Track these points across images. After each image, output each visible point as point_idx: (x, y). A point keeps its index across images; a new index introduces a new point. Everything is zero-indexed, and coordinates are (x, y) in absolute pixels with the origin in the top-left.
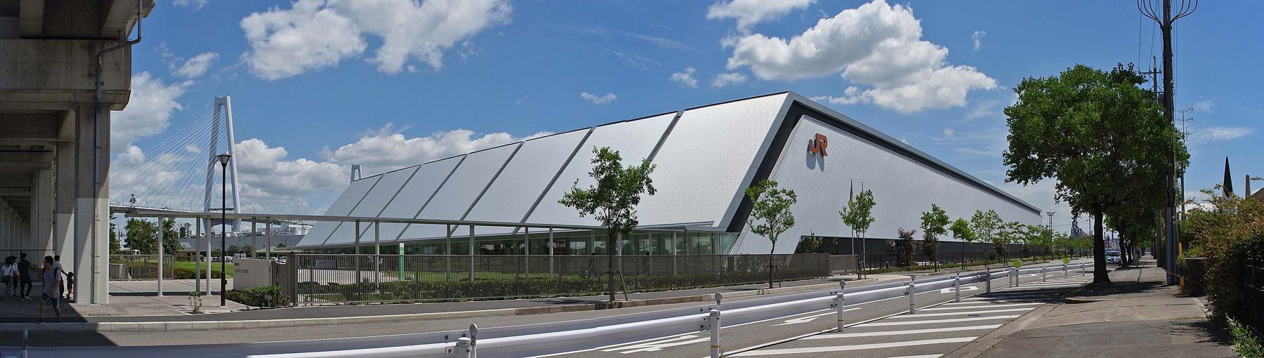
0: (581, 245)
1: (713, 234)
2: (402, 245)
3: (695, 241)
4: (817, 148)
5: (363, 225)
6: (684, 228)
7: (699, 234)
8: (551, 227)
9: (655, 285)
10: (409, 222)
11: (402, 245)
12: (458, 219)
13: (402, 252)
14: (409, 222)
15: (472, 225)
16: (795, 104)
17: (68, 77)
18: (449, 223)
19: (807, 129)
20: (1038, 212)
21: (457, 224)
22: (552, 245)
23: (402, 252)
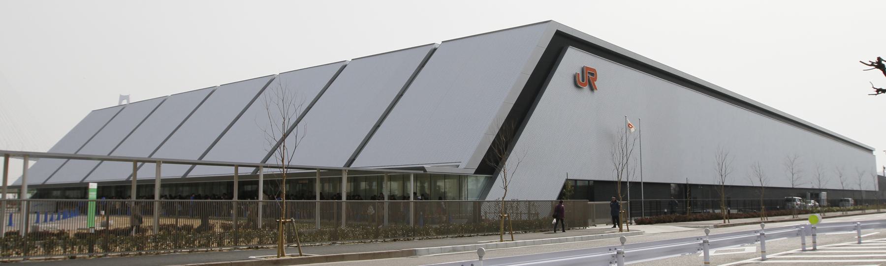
0: (395, 187)
1: (460, 179)
2: (93, 186)
3: (440, 183)
4: (586, 80)
5: (11, 160)
6: (423, 169)
7: (445, 176)
8: (237, 166)
9: (403, 235)
10: (103, 159)
11: (93, 186)
12: (145, 156)
13: (93, 195)
14: (103, 159)
15: (158, 162)
16: (559, 34)
17: (763, 212)
18: (135, 161)
19: (573, 60)
20: (870, 151)
21: (144, 161)
22: (345, 188)
23: (93, 195)
